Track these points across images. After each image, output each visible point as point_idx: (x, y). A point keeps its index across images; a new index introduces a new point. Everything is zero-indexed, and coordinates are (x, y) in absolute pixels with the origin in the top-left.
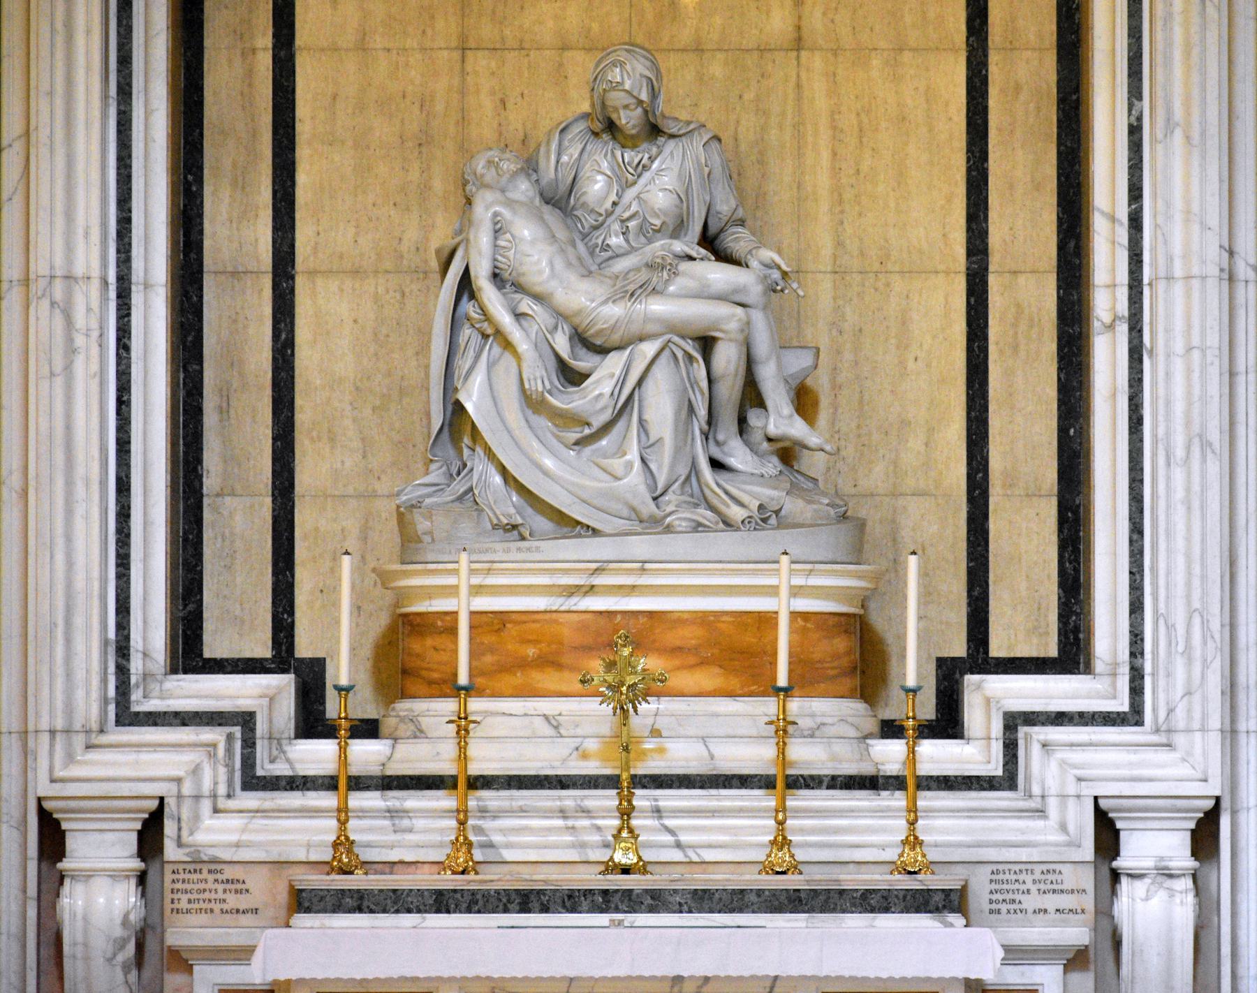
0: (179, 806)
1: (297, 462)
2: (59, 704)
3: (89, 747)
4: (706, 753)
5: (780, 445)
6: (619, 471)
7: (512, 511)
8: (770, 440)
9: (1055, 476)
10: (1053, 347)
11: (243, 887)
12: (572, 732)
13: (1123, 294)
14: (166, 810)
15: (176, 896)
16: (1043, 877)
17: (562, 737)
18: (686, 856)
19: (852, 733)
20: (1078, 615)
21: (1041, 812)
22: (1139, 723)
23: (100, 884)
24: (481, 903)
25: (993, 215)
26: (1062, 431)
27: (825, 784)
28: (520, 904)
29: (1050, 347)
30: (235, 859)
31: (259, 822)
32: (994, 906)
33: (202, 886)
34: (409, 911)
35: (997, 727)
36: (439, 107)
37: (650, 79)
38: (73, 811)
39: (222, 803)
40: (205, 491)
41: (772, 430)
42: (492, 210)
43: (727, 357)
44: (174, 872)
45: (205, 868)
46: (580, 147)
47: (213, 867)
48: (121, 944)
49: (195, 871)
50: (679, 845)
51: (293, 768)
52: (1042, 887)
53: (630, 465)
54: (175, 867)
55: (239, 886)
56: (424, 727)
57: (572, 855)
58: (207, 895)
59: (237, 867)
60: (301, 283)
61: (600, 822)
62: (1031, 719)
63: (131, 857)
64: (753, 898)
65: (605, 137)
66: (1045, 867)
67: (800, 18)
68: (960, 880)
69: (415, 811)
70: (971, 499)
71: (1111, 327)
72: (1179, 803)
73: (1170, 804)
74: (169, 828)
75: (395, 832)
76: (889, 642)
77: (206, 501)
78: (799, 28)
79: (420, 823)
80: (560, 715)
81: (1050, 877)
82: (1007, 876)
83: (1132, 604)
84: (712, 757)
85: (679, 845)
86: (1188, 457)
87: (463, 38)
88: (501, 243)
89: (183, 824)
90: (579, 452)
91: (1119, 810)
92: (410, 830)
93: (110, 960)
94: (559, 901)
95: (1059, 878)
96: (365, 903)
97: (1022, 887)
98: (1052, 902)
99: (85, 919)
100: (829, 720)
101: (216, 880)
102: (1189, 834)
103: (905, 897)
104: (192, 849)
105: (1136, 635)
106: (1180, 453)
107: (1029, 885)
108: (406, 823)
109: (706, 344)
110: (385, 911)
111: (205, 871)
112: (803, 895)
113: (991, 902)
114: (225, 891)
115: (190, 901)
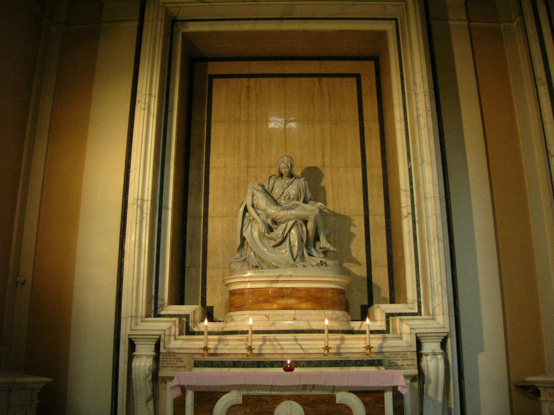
0: (165, 337)
1: (208, 260)
2: (134, 309)
3: (142, 321)
4: (308, 325)
5: (324, 250)
6: (284, 253)
7: (257, 263)
8: (321, 248)
9: (387, 262)
10: (385, 232)
11: (182, 360)
12: (272, 319)
13: (410, 208)
14: (161, 339)
15: (163, 362)
16: (403, 356)
17: (269, 320)
18: (304, 352)
19: (345, 319)
20: (393, 294)
21: (400, 338)
22: (421, 315)
23: (144, 358)
24: (246, 365)
25: (369, 202)
26: (388, 251)
27: (340, 332)
28: (257, 365)
29: (384, 232)
30: (179, 352)
31: (187, 343)
32: (390, 364)
33: (170, 360)
34: (226, 367)
35: (384, 317)
36: (242, 180)
37: (290, 161)
38: (137, 339)
39: (177, 337)
40: (186, 267)
41: (322, 246)
42: (252, 191)
43: (310, 225)
44: (163, 356)
45: (172, 355)
46: (274, 181)
47: (173, 354)
48: (147, 376)
49: (169, 355)
50: (302, 349)
51: (199, 330)
52: (403, 358)
53: (286, 251)
54: (163, 354)
55: (180, 360)
56: (234, 318)
57: (273, 352)
58: (172, 362)
59: (180, 354)
60: (209, 219)
61: (280, 342)
62: (393, 315)
63: (153, 352)
64: (324, 363)
65: (280, 178)
66: (403, 353)
67: (324, 160)
68: (443, 336)
69: (229, 339)
70: (367, 267)
71: (406, 217)
72: (438, 334)
73: (435, 335)
74: (162, 344)
75: (224, 345)
76: (349, 301)
77: (186, 269)
78: (323, 162)
79: (230, 343)
80: (269, 314)
81: (404, 356)
82: (392, 356)
83: (417, 284)
84: (310, 325)
85: (302, 349)
86: (434, 243)
87: (248, 165)
88: (254, 198)
89: (166, 342)
90: (274, 249)
91: (422, 337)
92: (228, 345)
93: (146, 379)
94: (268, 364)
95: (407, 356)
96: (214, 365)
97: (397, 359)
98: (406, 363)
99: (139, 368)
100: (339, 316)
101: (174, 358)
102: (440, 343)
103: (367, 362)
104: (168, 349)
105: (419, 293)
106: (432, 242)
107: (399, 358)
108: (227, 343)
109: (306, 222)
110: (219, 367)
111: (171, 356)
112: (338, 362)
113: (389, 363)
114: (176, 361)
115: (167, 364)
